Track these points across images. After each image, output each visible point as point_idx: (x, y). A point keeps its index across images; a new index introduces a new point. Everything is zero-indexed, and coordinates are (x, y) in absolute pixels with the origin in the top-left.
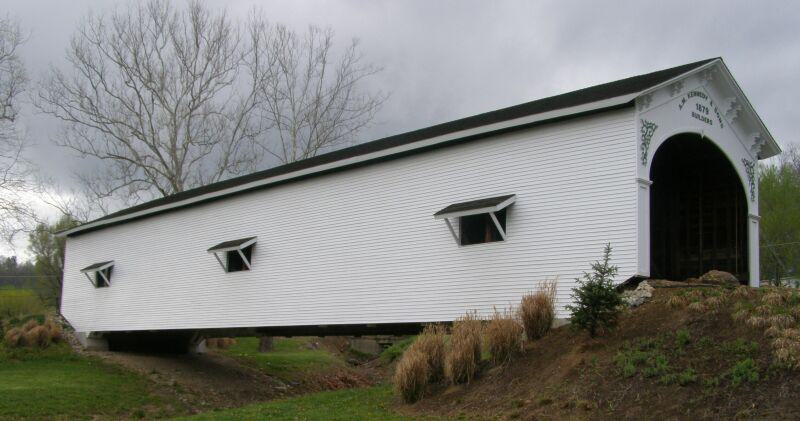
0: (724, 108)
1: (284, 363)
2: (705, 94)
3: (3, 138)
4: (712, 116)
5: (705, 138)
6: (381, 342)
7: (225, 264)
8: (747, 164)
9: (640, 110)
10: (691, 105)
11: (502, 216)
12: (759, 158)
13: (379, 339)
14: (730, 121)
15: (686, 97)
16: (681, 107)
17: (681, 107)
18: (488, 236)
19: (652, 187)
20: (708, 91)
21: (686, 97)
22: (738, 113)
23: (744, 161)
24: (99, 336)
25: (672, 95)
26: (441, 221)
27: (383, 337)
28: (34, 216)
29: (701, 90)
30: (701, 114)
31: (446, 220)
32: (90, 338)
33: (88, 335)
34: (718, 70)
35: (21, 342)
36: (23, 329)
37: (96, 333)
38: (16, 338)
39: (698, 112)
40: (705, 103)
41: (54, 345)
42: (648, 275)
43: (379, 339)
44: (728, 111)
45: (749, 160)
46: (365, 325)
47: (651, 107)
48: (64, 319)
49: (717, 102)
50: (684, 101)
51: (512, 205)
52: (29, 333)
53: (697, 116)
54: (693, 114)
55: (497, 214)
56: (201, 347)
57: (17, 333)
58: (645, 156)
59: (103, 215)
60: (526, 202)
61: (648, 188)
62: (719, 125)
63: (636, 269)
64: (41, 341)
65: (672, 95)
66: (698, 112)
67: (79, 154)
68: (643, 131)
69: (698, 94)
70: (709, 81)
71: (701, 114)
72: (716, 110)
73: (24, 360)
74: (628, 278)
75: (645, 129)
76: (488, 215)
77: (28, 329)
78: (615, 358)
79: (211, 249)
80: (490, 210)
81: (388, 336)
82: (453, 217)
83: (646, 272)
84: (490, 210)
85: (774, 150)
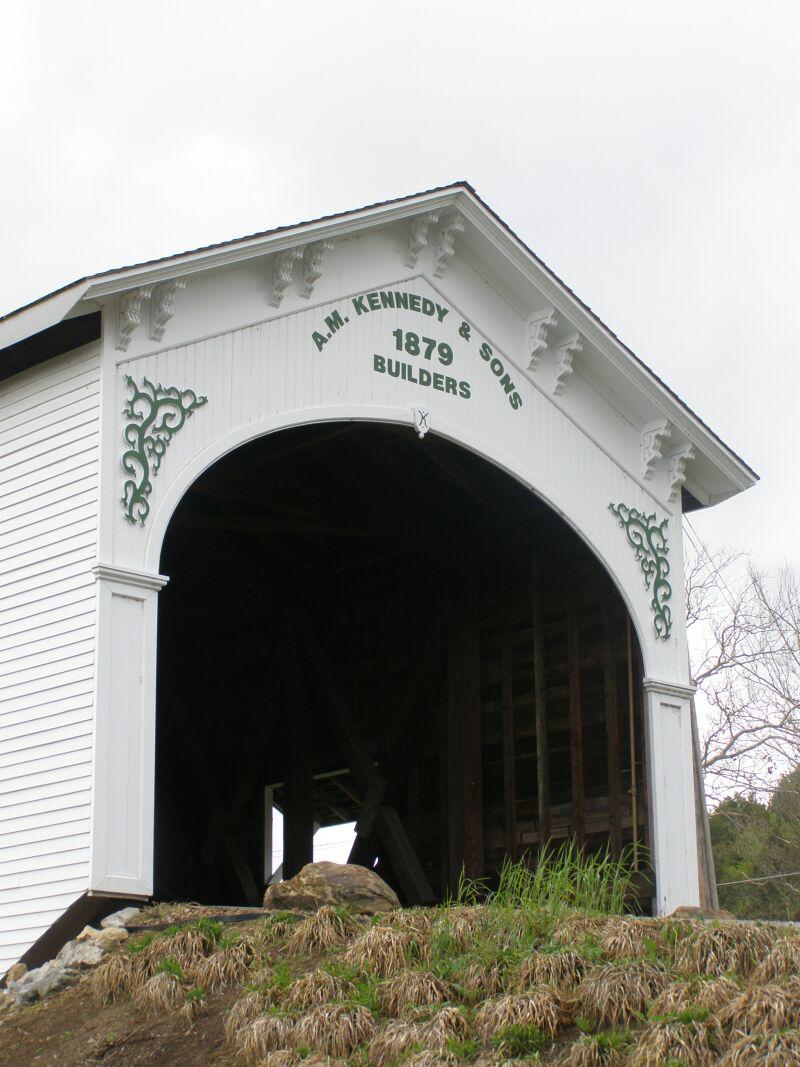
0: (518, 351)
2: (436, 299)
3: (253, 1062)
4: (467, 364)
8: (630, 519)
9: (122, 344)
10: (376, 331)
12: (690, 503)
14: (552, 385)
15: (346, 310)
16: (320, 340)
17: (320, 340)
19: (165, 596)
20: (449, 290)
21: (346, 310)
22: (577, 359)
23: (616, 510)
25: (275, 301)
28: (665, 541)
30: (417, 363)
34: (466, 223)
39: (404, 357)
40: (444, 331)
42: (148, 890)
45: (645, 508)
47: (168, 339)
49: (486, 326)
50: (335, 322)
58: (140, 495)
61: (157, 594)
62: (504, 398)
63: (87, 870)
65: (275, 301)
66: (404, 357)
69: (408, 301)
70: (444, 260)
71: (417, 363)
72: (485, 351)
83: (137, 875)
85: (740, 483)
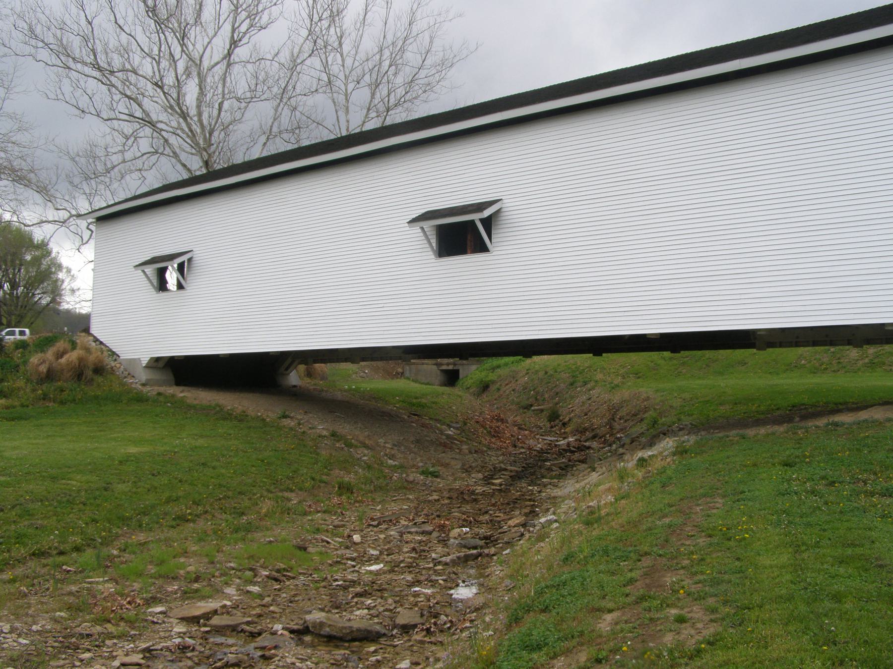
1: (416, 398)
6: (444, 367)
7: (155, 284)
11: (488, 223)
13: (441, 364)
18: (469, 251)
24: (161, 364)
26: (416, 230)
27: (445, 361)
31: (422, 228)
32: (147, 367)
33: (144, 363)
35: (50, 376)
36: (50, 354)
37: (158, 359)
38: (43, 369)
41: (100, 379)
43: (441, 364)
46: (218, 355)
48: (96, 340)
51: (498, 212)
52: (63, 360)
55: (482, 220)
56: (294, 378)
57: (44, 362)
59: (185, 176)
60: (512, 205)
64: (79, 373)
67: (78, 112)
73: (62, 403)
76: (472, 222)
77: (60, 355)
79: (137, 266)
80: (475, 217)
81: (451, 360)
82: (428, 225)
84: (475, 217)
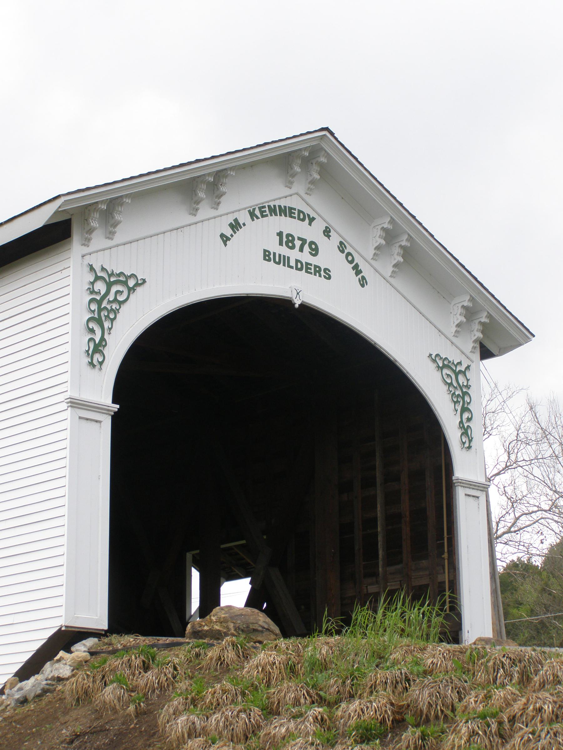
2: (307, 210)
5: (303, 306)
12: (486, 354)
14: (388, 270)
15: (244, 217)
16: (225, 239)
19: (116, 419)
21: (244, 217)
25: (194, 211)
29: (295, 203)
34: (328, 156)
39: (284, 251)
42: (104, 625)
44: (378, 248)
47: (119, 238)
49: (351, 237)
50: (235, 226)
53: (283, 261)
54: (534, 336)
61: (110, 417)
63: (61, 611)
65: (194, 211)
66: (284, 251)
68: (92, 292)
69: (287, 212)
70: (312, 182)
71: (294, 255)
72: (342, 247)
74: (37, 645)
75: (100, 287)
78: (473, 702)
